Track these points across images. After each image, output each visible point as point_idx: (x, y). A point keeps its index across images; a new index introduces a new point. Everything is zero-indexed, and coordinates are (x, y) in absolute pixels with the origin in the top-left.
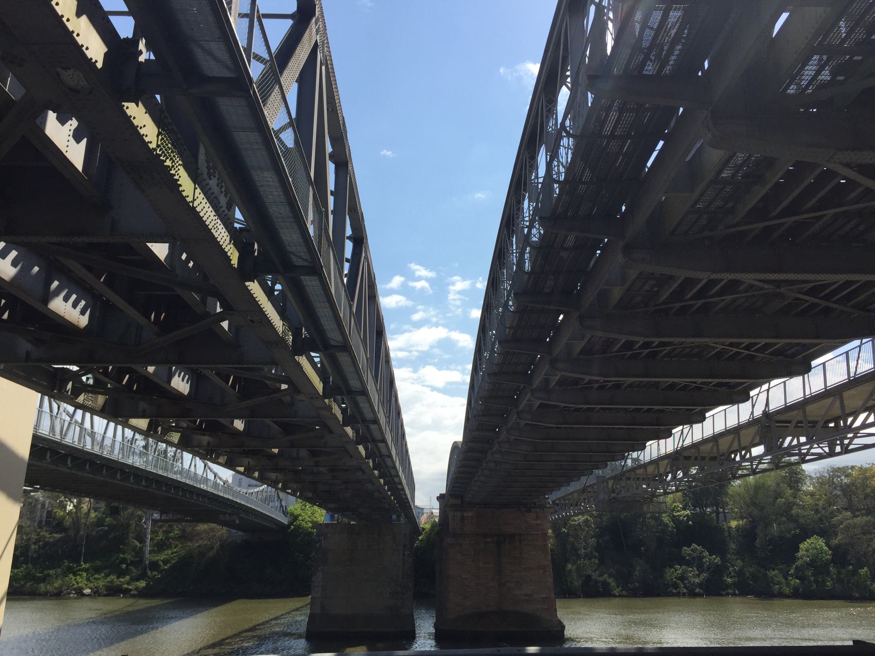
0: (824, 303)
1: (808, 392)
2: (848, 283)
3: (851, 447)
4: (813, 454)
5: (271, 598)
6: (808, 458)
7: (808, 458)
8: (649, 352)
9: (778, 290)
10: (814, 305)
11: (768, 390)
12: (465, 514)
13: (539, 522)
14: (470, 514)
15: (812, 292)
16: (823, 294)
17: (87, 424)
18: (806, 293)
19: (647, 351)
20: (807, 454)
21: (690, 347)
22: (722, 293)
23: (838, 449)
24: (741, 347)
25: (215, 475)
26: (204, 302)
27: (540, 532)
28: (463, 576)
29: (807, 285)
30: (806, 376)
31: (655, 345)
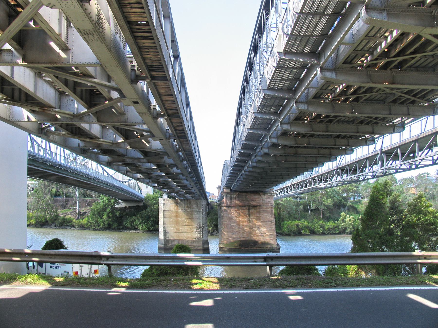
0: (413, 98)
1: (402, 140)
2: (423, 90)
3: (419, 166)
4: (402, 169)
5: (21, 85)
6: (399, 171)
7: (399, 171)
8: (329, 120)
9: (392, 92)
10: (408, 99)
11: (378, 140)
12: (232, 196)
13: (269, 200)
14: (235, 196)
15: (407, 93)
16: (413, 94)
17: (48, 148)
18: (405, 93)
19: (328, 119)
20: (398, 169)
21: (349, 118)
22: (365, 92)
23: (413, 167)
24: (378, 119)
25: (108, 173)
26: (109, 93)
27: (269, 205)
28: (232, 224)
29: (406, 90)
30: (401, 133)
31: (331, 116)
